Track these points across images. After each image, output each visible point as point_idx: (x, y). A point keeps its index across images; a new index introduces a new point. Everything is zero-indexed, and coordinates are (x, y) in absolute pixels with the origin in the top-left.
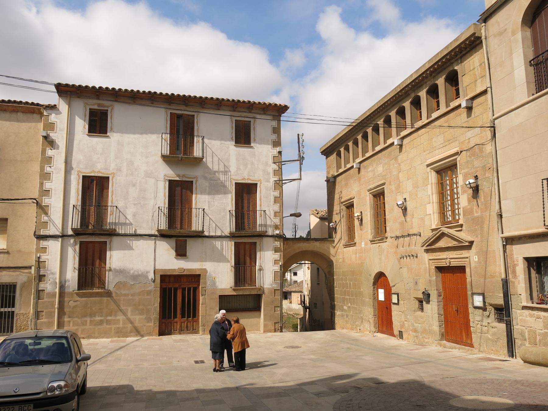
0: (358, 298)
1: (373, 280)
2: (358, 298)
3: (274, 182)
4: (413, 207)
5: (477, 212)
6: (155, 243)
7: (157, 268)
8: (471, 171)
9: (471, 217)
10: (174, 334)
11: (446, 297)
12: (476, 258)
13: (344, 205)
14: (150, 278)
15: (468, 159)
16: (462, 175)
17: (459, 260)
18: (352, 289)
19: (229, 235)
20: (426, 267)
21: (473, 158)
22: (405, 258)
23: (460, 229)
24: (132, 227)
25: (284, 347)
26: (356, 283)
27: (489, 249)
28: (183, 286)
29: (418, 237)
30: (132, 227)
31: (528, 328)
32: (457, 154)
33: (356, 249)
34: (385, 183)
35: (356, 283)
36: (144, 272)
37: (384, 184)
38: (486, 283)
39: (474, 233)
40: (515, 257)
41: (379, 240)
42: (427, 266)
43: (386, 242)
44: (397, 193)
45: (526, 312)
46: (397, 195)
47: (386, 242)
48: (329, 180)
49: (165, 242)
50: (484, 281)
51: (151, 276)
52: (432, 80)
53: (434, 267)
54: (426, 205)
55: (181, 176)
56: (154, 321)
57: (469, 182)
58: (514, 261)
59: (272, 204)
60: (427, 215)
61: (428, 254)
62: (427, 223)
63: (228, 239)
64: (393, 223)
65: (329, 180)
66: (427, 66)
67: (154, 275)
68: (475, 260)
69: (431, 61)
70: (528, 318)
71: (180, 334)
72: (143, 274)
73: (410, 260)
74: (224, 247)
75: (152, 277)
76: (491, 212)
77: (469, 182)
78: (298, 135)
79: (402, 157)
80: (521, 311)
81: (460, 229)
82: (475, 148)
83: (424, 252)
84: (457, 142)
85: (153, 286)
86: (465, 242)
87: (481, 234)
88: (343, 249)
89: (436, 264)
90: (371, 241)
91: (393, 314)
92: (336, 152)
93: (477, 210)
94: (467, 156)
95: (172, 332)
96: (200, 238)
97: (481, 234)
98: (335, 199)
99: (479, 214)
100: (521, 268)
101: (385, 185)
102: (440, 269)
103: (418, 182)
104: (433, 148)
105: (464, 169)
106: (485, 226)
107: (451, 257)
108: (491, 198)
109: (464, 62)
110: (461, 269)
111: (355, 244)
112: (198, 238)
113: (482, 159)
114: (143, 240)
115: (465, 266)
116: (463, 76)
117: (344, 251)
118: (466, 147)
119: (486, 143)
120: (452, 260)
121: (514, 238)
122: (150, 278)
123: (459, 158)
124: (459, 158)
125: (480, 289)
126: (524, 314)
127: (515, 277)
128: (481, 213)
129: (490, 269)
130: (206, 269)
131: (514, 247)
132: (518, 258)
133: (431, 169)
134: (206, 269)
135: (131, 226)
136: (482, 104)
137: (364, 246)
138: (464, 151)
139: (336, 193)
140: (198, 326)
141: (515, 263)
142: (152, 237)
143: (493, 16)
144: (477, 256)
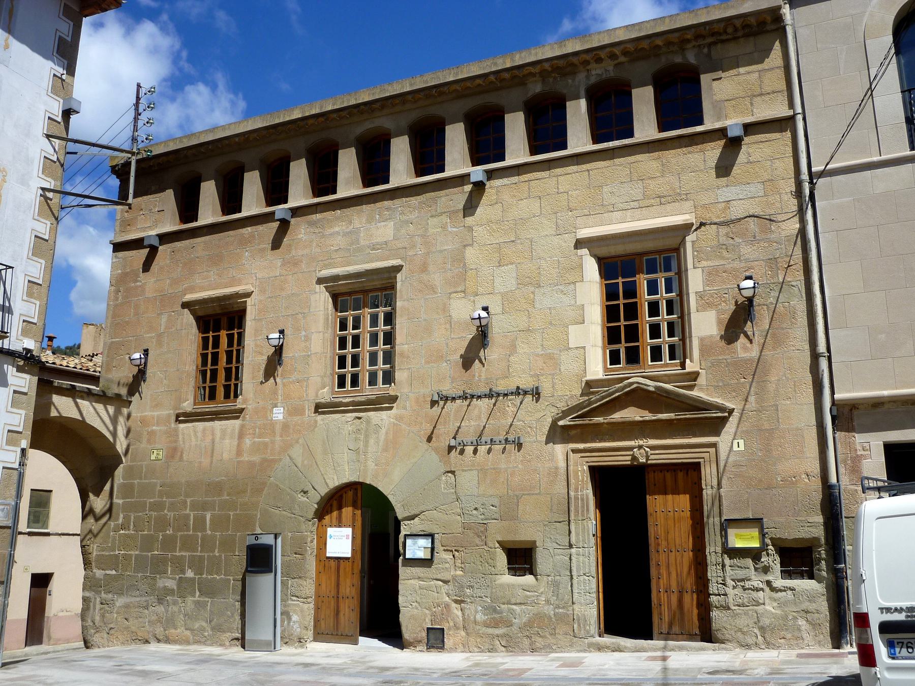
1: (316, 506)
3: (40, 192)
16: (703, 270)
18: (209, 532)
29: (529, 398)
35: (231, 513)
42: (562, 464)
44: (450, 293)
46: (450, 298)
53: (585, 468)
57: (479, 315)
59: (25, 256)
60: (570, 349)
62: (568, 365)
69: (637, 27)
77: (479, 315)
78: (139, 86)
88: (173, 425)
89: (587, 459)
91: (400, 587)
104: (602, 205)
113: (766, 245)
115: (699, 463)
116: (714, 80)
118: (718, 217)
132: (869, 442)
136: (770, 141)
137: (281, 417)
141: (859, 453)
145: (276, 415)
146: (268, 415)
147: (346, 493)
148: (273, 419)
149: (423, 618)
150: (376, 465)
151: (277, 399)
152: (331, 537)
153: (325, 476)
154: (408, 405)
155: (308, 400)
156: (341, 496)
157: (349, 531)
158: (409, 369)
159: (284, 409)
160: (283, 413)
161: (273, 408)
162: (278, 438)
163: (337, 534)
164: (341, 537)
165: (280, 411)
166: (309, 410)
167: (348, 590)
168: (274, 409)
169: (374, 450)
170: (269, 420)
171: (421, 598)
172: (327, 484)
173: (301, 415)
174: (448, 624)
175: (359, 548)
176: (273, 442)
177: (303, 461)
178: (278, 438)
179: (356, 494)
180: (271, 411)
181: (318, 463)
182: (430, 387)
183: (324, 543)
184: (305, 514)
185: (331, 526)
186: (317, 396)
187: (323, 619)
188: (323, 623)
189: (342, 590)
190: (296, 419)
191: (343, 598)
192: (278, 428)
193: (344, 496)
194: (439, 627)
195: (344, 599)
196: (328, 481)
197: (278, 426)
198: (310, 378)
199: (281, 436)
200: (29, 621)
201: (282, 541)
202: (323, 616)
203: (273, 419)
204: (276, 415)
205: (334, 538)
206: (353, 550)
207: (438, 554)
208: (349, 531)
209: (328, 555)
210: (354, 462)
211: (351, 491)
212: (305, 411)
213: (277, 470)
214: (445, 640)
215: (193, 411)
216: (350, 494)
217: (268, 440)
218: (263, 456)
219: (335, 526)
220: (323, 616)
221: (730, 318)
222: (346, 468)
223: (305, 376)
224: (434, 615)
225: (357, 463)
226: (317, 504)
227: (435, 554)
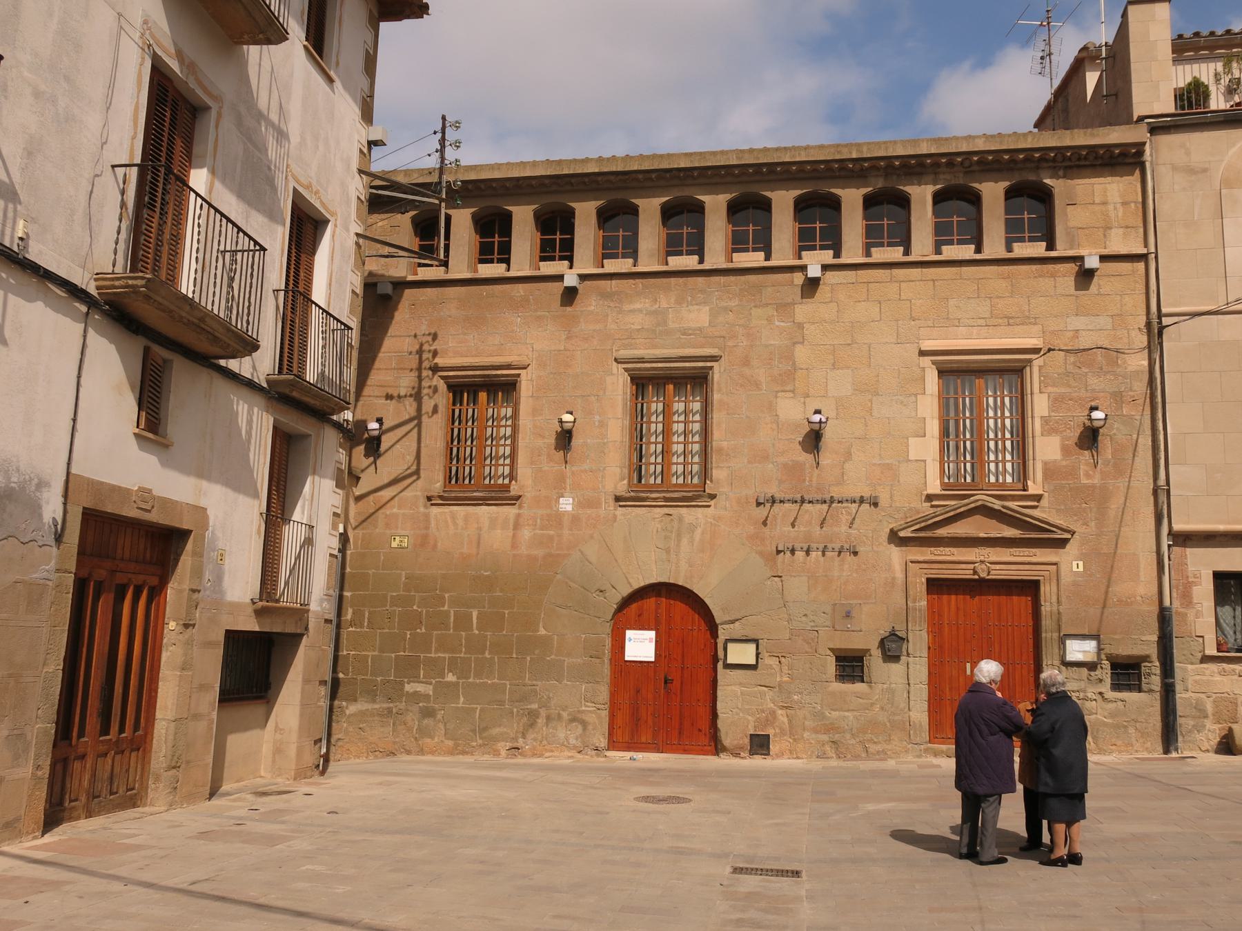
0: (514, 656)
2: (514, 656)
4: (852, 436)
5: (1088, 476)
6: (85, 331)
7: (74, 471)
8: (1077, 394)
9: (1069, 484)
10: (70, 819)
11: (941, 647)
12: (1078, 566)
13: (442, 377)
14: (48, 516)
15: (1070, 368)
16: (1049, 396)
17: (1027, 567)
19: (265, 385)
20: (894, 578)
21: (1085, 370)
22: (800, 555)
23: (1036, 504)
24: (15, 210)
25: (608, 813)
26: (507, 612)
27: (1119, 551)
28: (120, 578)
30: (15, 210)
31: (1214, 696)
32: (1036, 351)
33: (518, 516)
34: (721, 357)
36: (31, 480)
37: (715, 358)
38: (1105, 615)
39: (1075, 515)
40: (1191, 568)
41: (666, 499)
43: (709, 506)
45: (1213, 667)
47: (709, 506)
48: (375, 285)
49: (112, 348)
50: (1099, 611)
51: (52, 507)
52: (961, 175)
53: (924, 580)
54: (907, 438)
55: (186, 64)
56: (35, 755)
58: (1188, 577)
60: (910, 461)
61: (904, 548)
63: (259, 400)
64: (749, 462)
65: (375, 285)
66: (981, 146)
67: (65, 504)
68: (1075, 569)
70: (1218, 678)
71: (89, 815)
72: (24, 487)
73: (822, 559)
74: (254, 427)
75: (54, 511)
76: (1132, 482)
79: (804, 310)
80: (1197, 666)
81: (1036, 504)
82: (1095, 353)
83: (886, 543)
84: (1036, 327)
85: (52, 565)
86: (1060, 532)
87: (1096, 519)
90: (618, 499)
92: (416, 212)
93: (1091, 472)
94: (1068, 362)
95: (63, 811)
96: (205, 369)
97: (1096, 519)
98: (383, 349)
99: (1096, 480)
100: (1204, 591)
101: (717, 361)
102: (935, 586)
103: (878, 381)
105: (1053, 386)
106: (1112, 507)
107: (994, 558)
108: (1134, 457)
109: (1076, 180)
110: (1030, 588)
111: (1039, 501)
112: (201, 368)
114: (47, 305)
117: (427, 516)
118: (1066, 345)
119: (1126, 351)
120: (993, 567)
121: (1192, 535)
122: (48, 516)
123: (1038, 362)
124: (1038, 362)
125: (1086, 626)
126: (1207, 672)
127: (1187, 605)
128: (1102, 479)
129: (1120, 589)
130: (206, 509)
131: (1188, 550)
133: (934, 363)
134: (206, 509)
135: (11, 206)
137: (569, 508)
138: (1059, 350)
139: (389, 334)
140: (143, 769)
141: (1190, 580)
142: (77, 305)
143: (1172, 131)
144: (1081, 563)
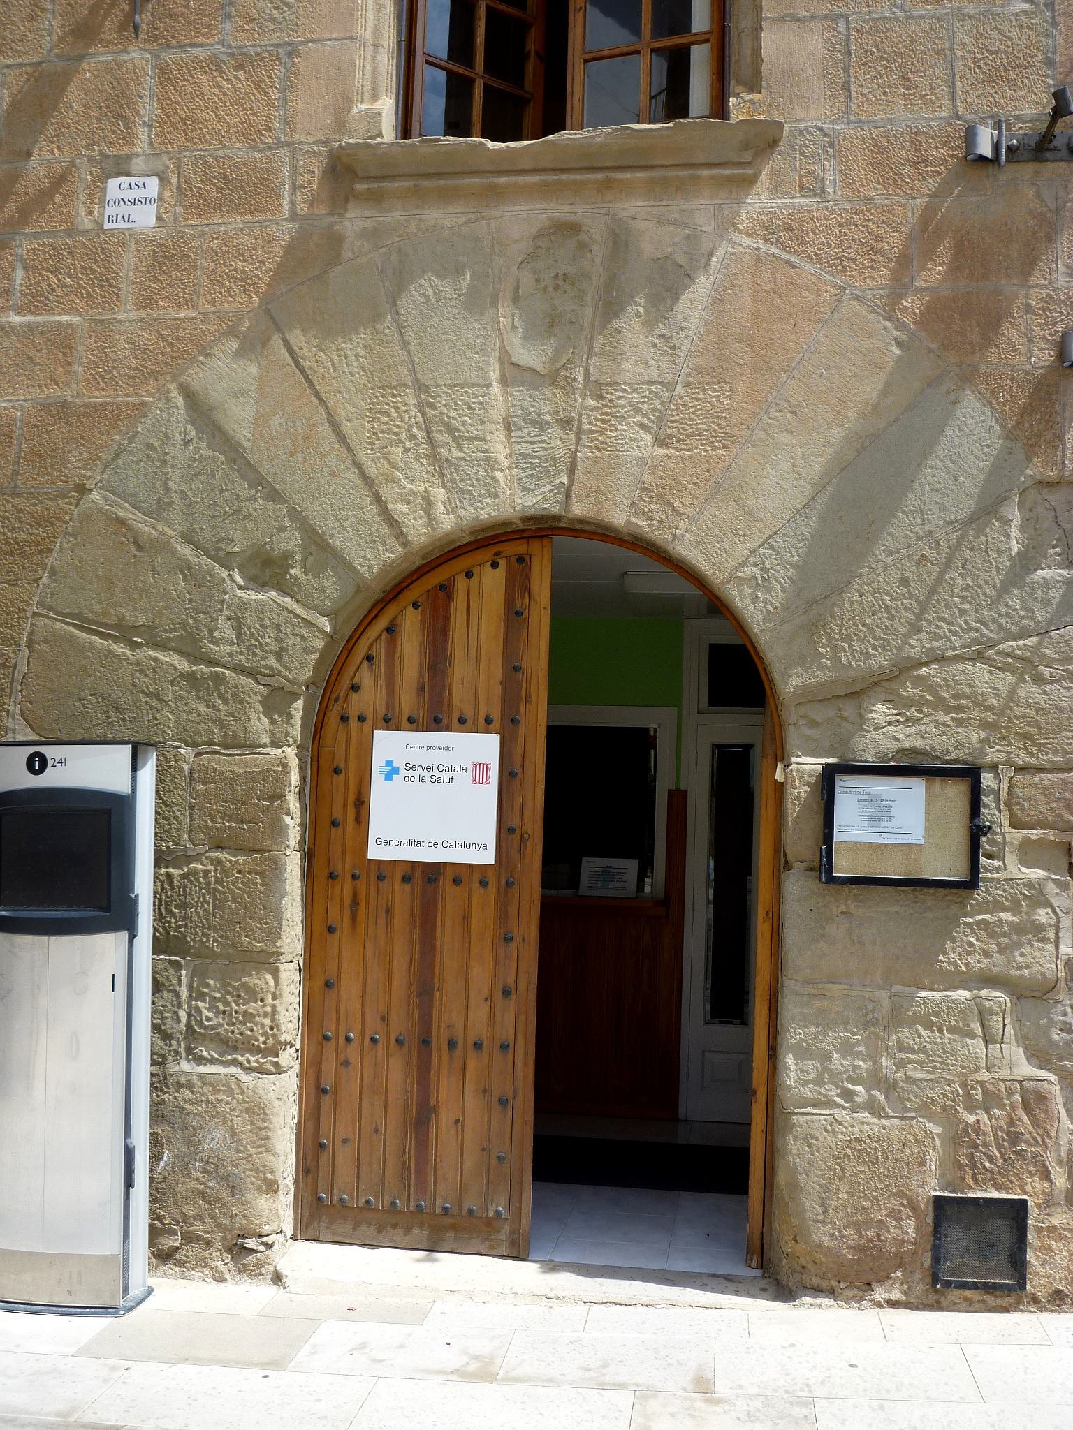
137: (145, 218)
145: (122, 210)
146: (82, 211)
147: (469, 575)
148: (106, 226)
149: (912, 1151)
150: (661, 442)
151: (128, 140)
152: (391, 771)
153: (385, 491)
154: (829, 177)
155: (288, 144)
156: (446, 589)
157: (486, 747)
158: (834, 18)
159: (163, 180)
160: (160, 199)
161: (106, 176)
162: (130, 313)
163: (433, 758)
164: (448, 775)
165: (140, 194)
166: (295, 188)
167: (479, 1014)
168: (113, 183)
169: (652, 374)
170: (85, 232)
171: (900, 1065)
172: (391, 521)
173: (257, 210)
174: (1040, 1185)
175: (533, 823)
176: (100, 328)
177: (261, 418)
178: (130, 313)
179: (519, 580)
180: (97, 193)
181: (346, 427)
182: (946, 101)
183: (352, 797)
184: (272, 661)
185: (389, 723)
186: (341, 125)
187: (345, 1141)
188: (344, 1156)
189: (448, 1016)
190: (225, 223)
191: (452, 1044)
192: (128, 265)
193: (461, 584)
194: (996, 1195)
195: (459, 1051)
196: (398, 508)
197: (129, 258)
198: (304, 48)
199: (147, 302)
200: (504, 802)
201: (160, 781)
202: (345, 1129)
203: (106, 226)
204: (122, 210)
205: (410, 779)
206: (504, 830)
207: (996, 863)
208: (486, 747)
209: (375, 852)
210: (541, 425)
211: (495, 565)
212: (275, 191)
213: (124, 457)
214: (1030, 1256)
215: (394, 96)
216: (492, 582)
217: (74, 319)
218: (51, 393)
219: (414, 724)
220: (345, 1129)
221: (68, 84)
222: (500, 450)
223: (278, 37)
224: (959, 1137)
225: (556, 431)
226: (332, 615)
227: (983, 860)
